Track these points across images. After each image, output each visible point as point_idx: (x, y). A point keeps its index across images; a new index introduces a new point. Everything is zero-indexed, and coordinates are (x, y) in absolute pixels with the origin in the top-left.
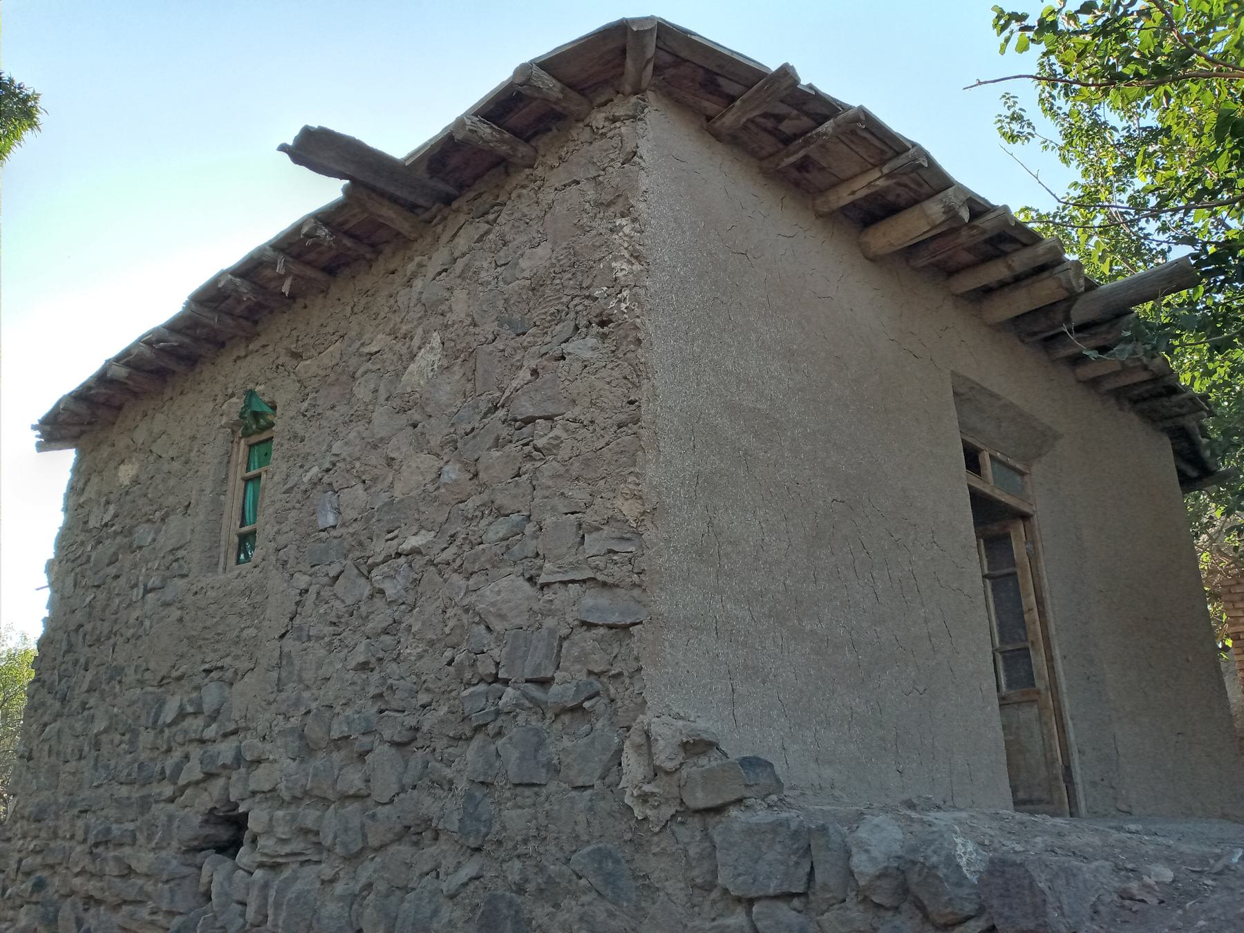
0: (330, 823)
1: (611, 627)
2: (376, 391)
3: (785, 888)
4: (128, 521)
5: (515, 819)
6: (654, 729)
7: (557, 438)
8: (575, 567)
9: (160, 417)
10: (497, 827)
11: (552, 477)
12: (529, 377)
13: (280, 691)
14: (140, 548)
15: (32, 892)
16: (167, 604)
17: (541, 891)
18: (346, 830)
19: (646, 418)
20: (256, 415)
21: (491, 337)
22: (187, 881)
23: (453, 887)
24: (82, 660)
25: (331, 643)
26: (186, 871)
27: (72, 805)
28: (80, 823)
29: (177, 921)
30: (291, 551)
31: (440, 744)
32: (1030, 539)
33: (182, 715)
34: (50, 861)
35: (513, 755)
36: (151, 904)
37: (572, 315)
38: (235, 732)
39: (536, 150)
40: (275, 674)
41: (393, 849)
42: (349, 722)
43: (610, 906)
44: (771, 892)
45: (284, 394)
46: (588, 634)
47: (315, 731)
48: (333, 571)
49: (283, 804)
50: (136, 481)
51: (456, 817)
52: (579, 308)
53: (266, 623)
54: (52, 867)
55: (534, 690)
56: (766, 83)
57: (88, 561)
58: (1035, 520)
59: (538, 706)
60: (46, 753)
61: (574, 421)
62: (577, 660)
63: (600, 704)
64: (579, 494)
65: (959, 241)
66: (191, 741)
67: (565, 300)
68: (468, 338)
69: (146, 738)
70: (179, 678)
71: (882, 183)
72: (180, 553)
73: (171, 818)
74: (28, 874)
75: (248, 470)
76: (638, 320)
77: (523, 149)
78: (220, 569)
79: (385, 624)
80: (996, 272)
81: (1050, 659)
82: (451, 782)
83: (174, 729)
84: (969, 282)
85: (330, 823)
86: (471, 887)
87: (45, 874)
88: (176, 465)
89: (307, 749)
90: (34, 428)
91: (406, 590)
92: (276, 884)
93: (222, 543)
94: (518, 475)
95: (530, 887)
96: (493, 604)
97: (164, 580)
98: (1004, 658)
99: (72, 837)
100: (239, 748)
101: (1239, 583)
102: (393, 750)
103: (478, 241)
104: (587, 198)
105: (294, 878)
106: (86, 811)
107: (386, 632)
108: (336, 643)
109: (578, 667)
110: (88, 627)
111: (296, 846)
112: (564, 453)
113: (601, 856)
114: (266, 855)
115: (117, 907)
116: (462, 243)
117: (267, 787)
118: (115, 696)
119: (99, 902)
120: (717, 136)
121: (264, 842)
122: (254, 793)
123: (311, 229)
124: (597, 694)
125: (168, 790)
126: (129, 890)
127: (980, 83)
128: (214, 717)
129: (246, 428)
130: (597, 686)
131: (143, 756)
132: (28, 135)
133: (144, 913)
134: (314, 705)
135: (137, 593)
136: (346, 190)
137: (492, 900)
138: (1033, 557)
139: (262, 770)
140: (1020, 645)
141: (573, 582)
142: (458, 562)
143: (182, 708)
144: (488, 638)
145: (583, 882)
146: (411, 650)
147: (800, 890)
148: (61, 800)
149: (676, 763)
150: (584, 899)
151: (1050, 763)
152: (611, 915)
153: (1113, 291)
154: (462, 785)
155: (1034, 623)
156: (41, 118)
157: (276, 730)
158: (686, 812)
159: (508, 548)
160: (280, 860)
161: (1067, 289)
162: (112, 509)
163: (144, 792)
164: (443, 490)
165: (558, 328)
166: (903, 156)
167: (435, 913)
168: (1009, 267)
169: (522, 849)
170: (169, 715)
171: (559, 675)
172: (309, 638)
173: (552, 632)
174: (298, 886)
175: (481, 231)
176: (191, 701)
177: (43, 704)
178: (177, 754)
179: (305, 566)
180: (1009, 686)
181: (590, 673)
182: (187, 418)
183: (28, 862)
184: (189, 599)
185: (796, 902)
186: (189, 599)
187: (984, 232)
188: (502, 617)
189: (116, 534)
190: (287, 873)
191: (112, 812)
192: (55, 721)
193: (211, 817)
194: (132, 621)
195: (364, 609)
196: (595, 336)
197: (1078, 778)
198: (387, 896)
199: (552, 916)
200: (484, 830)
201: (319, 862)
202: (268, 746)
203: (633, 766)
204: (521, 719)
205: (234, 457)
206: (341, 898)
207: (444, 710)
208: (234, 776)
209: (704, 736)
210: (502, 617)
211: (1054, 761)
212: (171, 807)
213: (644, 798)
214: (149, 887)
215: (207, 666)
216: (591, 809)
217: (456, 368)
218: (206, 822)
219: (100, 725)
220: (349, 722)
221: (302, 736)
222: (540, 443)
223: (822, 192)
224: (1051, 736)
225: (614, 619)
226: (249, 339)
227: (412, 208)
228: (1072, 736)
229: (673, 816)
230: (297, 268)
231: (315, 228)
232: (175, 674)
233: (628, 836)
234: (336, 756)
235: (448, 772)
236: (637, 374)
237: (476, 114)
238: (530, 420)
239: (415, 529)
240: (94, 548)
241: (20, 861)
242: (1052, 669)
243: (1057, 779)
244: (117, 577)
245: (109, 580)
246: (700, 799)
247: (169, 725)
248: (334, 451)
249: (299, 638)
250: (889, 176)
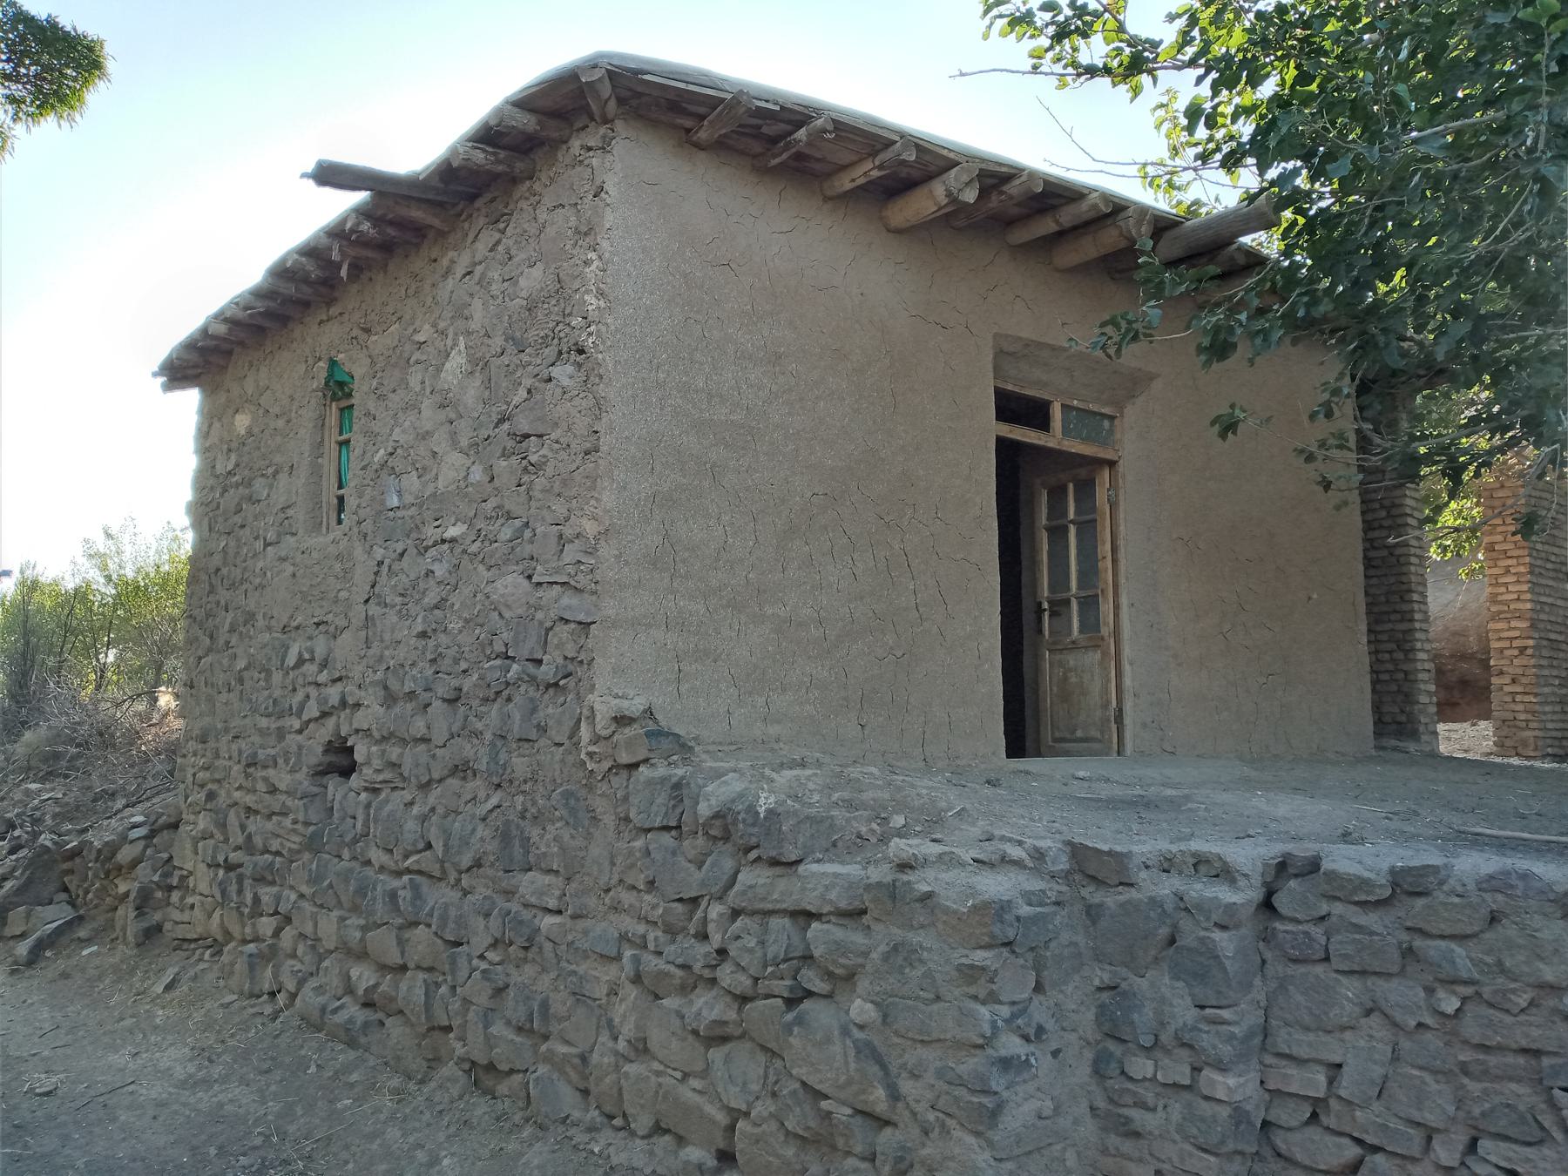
0: (410, 758)
1: (580, 623)
2: (423, 382)
3: (665, 823)
4: (246, 472)
5: (520, 765)
6: (597, 707)
7: (544, 456)
8: (557, 571)
9: (264, 370)
10: (509, 770)
11: (542, 491)
12: (525, 395)
13: (368, 648)
14: (259, 501)
15: (206, 801)
16: (283, 560)
17: (536, 818)
18: (417, 765)
19: (604, 448)
20: (341, 384)
21: (499, 350)
22: (318, 798)
23: (484, 812)
24: (223, 603)
25: (400, 611)
26: (316, 790)
27: (226, 730)
28: (234, 747)
29: (312, 828)
30: (367, 526)
31: (475, 703)
32: (1113, 486)
33: (301, 662)
34: (217, 776)
35: (517, 716)
36: (291, 816)
37: (556, 341)
38: (340, 679)
39: (534, 160)
40: (364, 633)
41: (450, 781)
42: (414, 679)
43: (572, 831)
44: (656, 825)
45: (357, 367)
46: (566, 627)
47: (394, 685)
48: (400, 547)
49: (378, 742)
50: (250, 433)
51: (485, 761)
52: (562, 335)
53: (354, 588)
54: (219, 781)
55: (531, 668)
56: (724, 109)
57: (218, 507)
58: (1121, 467)
59: (533, 679)
60: (203, 683)
61: (557, 442)
62: (557, 647)
63: (571, 682)
64: (560, 508)
65: (991, 205)
66: (309, 683)
67: (551, 325)
68: (484, 349)
69: (277, 677)
70: (297, 628)
71: (875, 173)
72: (290, 512)
73: (300, 747)
74: (202, 786)
75: (341, 433)
76: (600, 356)
77: (519, 166)
78: (324, 529)
79: (435, 601)
80: (1047, 226)
81: (1117, 607)
82: (481, 733)
83: (297, 672)
84: (1021, 235)
85: (410, 758)
86: (495, 814)
87: (213, 787)
88: (281, 423)
89: (390, 699)
90: (155, 375)
91: (450, 573)
92: (374, 805)
93: (324, 505)
94: (519, 485)
95: (528, 815)
96: (503, 596)
97: (279, 535)
98: (1079, 603)
99: (230, 758)
100: (342, 692)
101: (1502, 486)
102: (446, 705)
103: (491, 251)
104: (570, 225)
105: (387, 801)
106: (237, 737)
107: (436, 607)
108: (404, 612)
109: (558, 653)
110: (225, 571)
111: (387, 775)
112: (550, 470)
113: (568, 795)
114: (366, 781)
115: (269, 817)
116: (481, 248)
117: (366, 727)
118: (251, 638)
119: (257, 812)
120: (699, 146)
121: (365, 770)
122: (357, 731)
123: (353, 225)
124: (570, 674)
125: (297, 725)
126: (275, 803)
127: (962, 75)
128: (324, 665)
129: (334, 394)
130: (571, 667)
131: (277, 693)
132: (101, 85)
133: (287, 822)
134: (392, 663)
135: (259, 545)
136: (373, 197)
137: (507, 823)
138: (1113, 506)
139: (360, 713)
140: (1090, 593)
141: (556, 583)
142: (481, 556)
143: (300, 654)
144: (501, 623)
145: (557, 813)
146: (454, 626)
147: (674, 824)
148: (219, 726)
149: (609, 732)
150: (558, 825)
151: (1106, 705)
152: (572, 837)
153: (1194, 229)
154: (488, 736)
155: (1106, 571)
156: (110, 66)
157: (368, 680)
158: (617, 767)
159: (513, 549)
160: (377, 786)
161: (1126, 238)
162: (233, 457)
163: (279, 724)
164: (470, 489)
165: (547, 350)
166: (891, 149)
167: (474, 830)
168: (1057, 222)
169: (523, 787)
170: (291, 660)
171: (546, 658)
172: (386, 605)
173: (541, 623)
174: (389, 807)
175: (493, 240)
176: (306, 649)
177: (197, 639)
178: (300, 696)
179: (380, 541)
180: (1081, 632)
181: (566, 658)
182: (286, 376)
183: (201, 775)
184: (299, 557)
185: (674, 833)
186: (299, 557)
187: (1011, 197)
188: (508, 607)
189: (237, 485)
190: (383, 795)
191: (256, 739)
192: (207, 655)
193: (329, 748)
194: (257, 570)
195: (422, 585)
196: (573, 364)
197: (1127, 721)
198: (446, 817)
199: (542, 837)
200: (501, 771)
201: (403, 789)
202: (363, 693)
203: (585, 733)
204: (523, 689)
205: (327, 420)
206: (416, 818)
207: (476, 676)
208: (343, 715)
209: (627, 713)
210: (508, 607)
211: (1108, 702)
212: (299, 738)
213: (591, 755)
214: (289, 803)
215: (316, 620)
216: (562, 761)
217: (477, 374)
218: (326, 752)
219: (241, 664)
220: (414, 679)
221: (386, 688)
222: (533, 458)
223: (828, 176)
224: (1109, 681)
225: (582, 617)
226: (330, 303)
227: (441, 205)
228: (1128, 681)
229: (610, 769)
230: (352, 252)
231: (358, 224)
232: (295, 624)
233: (584, 782)
234: (409, 706)
235: (479, 726)
236: (599, 407)
237: (469, 140)
238: (527, 436)
239: (453, 520)
240: (222, 495)
241: (194, 775)
242: (1116, 615)
243: (1108, 720)
244: (243, 526)
245: (236, 529)
246: (625, 758)
247: (293, 668)
248: (395, 437)
249: (378, 604)
250: (881, 167)
